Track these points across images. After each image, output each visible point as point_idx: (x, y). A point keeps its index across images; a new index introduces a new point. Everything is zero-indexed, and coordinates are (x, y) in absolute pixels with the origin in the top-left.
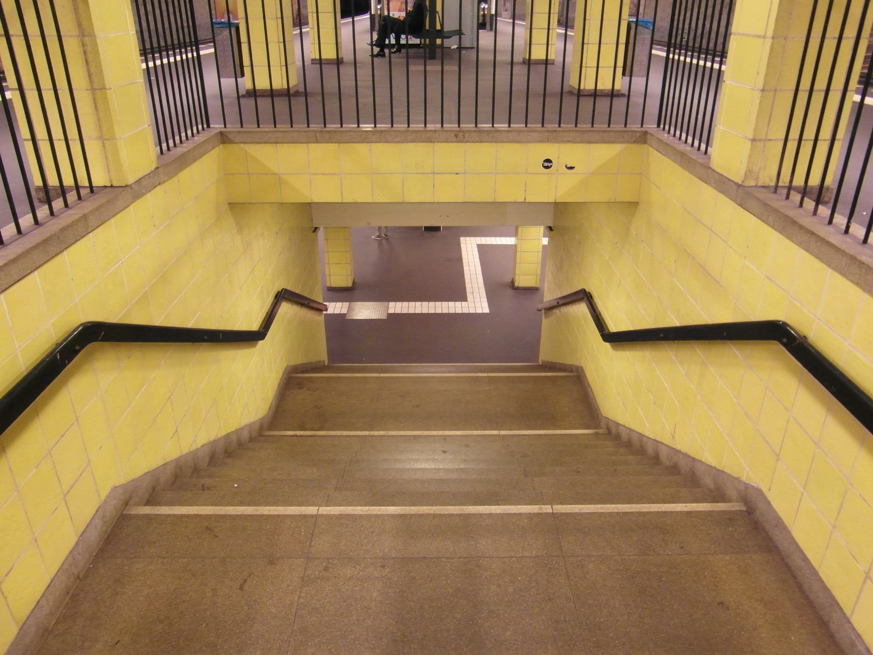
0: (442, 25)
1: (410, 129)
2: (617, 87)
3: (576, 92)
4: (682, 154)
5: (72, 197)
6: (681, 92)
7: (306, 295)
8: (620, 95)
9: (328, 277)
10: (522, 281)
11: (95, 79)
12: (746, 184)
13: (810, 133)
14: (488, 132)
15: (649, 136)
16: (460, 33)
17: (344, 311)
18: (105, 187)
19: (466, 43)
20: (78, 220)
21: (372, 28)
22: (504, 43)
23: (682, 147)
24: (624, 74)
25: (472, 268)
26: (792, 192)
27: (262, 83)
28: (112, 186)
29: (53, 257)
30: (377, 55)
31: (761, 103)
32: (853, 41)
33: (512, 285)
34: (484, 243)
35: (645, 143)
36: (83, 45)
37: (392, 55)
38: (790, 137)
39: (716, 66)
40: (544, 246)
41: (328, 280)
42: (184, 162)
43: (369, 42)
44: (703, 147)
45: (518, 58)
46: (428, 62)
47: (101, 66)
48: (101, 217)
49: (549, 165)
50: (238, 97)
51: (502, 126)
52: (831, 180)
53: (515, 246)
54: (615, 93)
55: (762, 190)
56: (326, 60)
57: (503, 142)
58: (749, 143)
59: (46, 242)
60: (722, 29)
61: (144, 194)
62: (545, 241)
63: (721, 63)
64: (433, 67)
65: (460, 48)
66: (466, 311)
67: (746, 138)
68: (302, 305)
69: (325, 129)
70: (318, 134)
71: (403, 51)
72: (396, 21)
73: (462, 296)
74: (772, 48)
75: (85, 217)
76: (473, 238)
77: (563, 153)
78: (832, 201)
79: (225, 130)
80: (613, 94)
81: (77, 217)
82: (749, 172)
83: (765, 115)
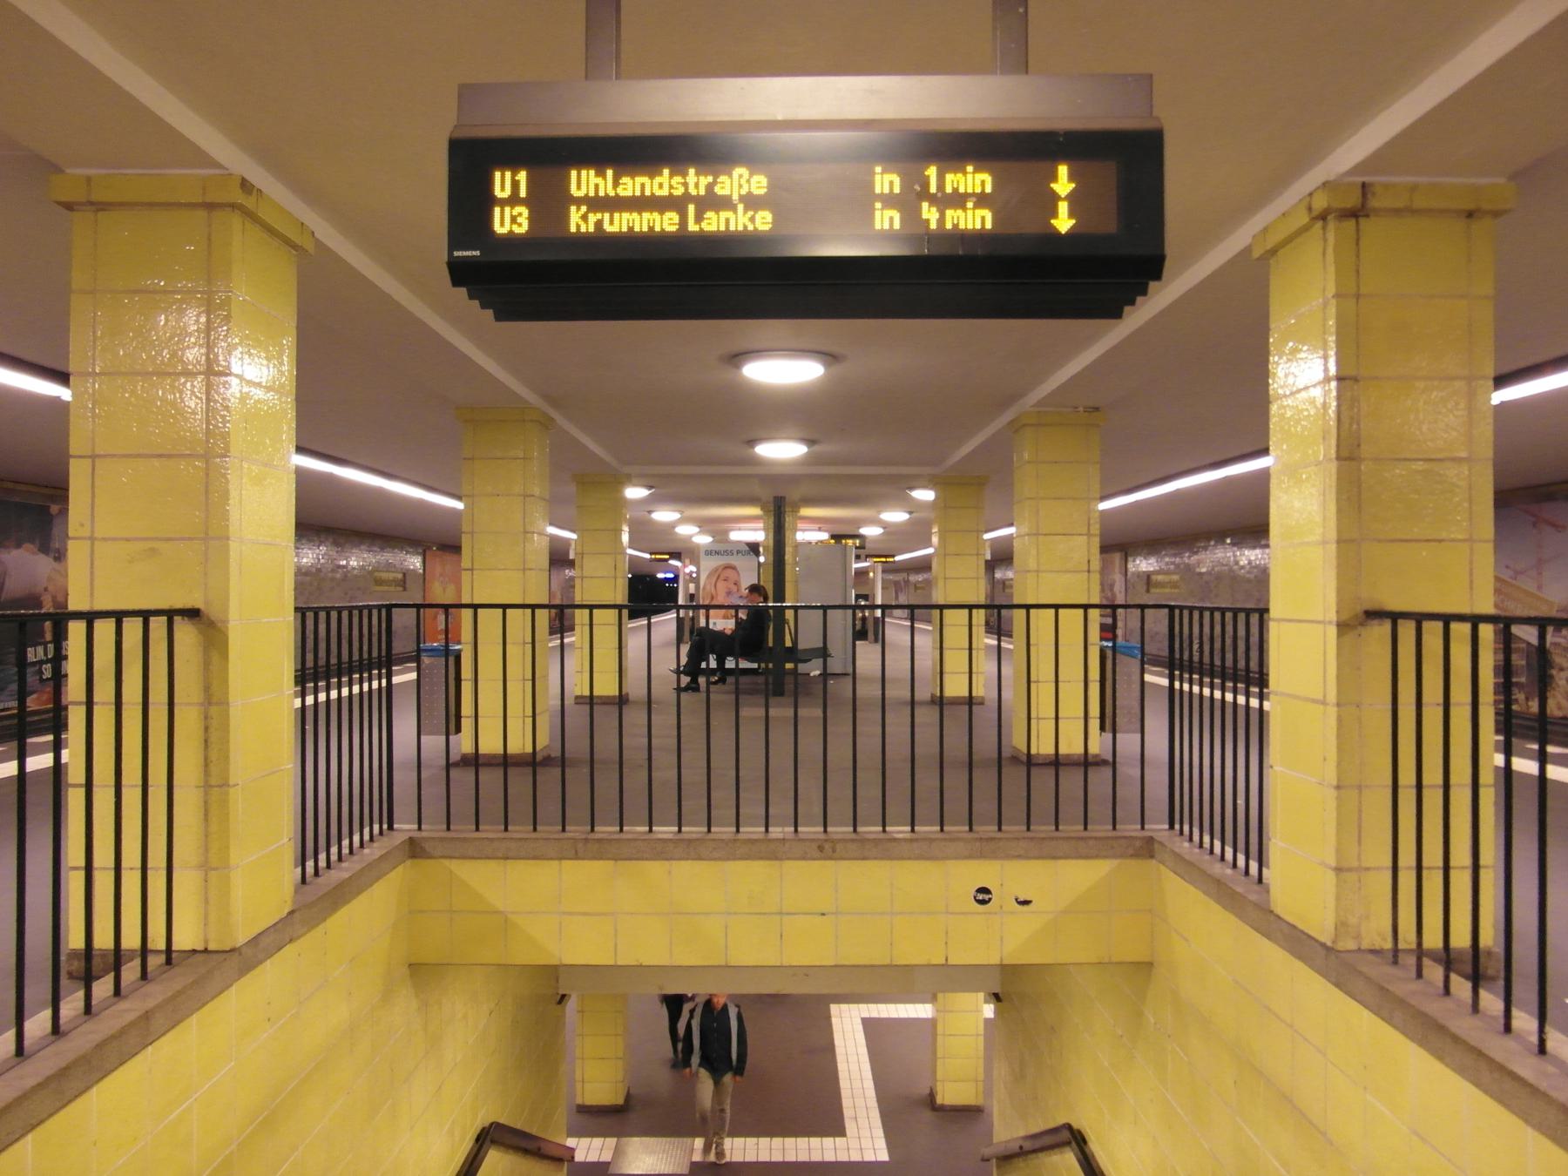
0: (795, 642)
1: (740, 836)
2: (1094, 748)
3: (1024, 758)
4: (1218, 882)
5: (130, 972)
6: (1202, 753)
7: (534, 1131)
8: (1100, 762)
9: (579, 1086)
10: (950, 1094)
11: (213, 769)
12: (1341, 946)
13: (1433, 856)
14: (876, 842)
15: (1156, 846)
16: (823, 653)
17: (606, 1157)
18: (194, 951)
19: (835, 665)
20: (132, 1024)
21: (679, 640)
22: (898, 665)
23: (1217, 869)
24: (1102, 728)
25: (854, 1067)
26: (1426, 962)
27: (491, 744)
28: (206, 951)
29: (70, 1102)
30: (687, 689)
31: (1339, 807)
32: (1468, 710)
33: (930, 1101)
34: (875, 1015)
35: (1152, 857)
36: (206, 718)
37: (712, 688)
38: (1401, 863)
39: (1254, 703)
40: (987, 1021)
41: (579, 1093)
42: (340, 896)
43: (674, 666)
44: (1254, 866)
45: (923, 694)
46: (772, 700)
47: (228, 751)
48: (175, 1012)
49: (986, 897)
50: (448, 766)
51: (900, 830)
52: (1490, 937)
53: (932, 1023)
54: (1090, 759)
55: (1370, 957)
56: (600, 697)
57: (903, 858)
58: (1331, 875)
59: (63, 1073)
60: (1254, 639)
61: (261, 962)
62: (989, 1010)
63: (1261, 697)
64: (781, 711)
65: (825, 675)
66: (843, 1157)
67: (1323, 864)
68: (526, 1152)
69: (592, 836)
70: (580, 845)
71: (730, 679)
72: (720, 635)
73: (833, 1125)
74: (1340, 720)
75: (147, 1016)
76: (853, 1006)
77: (1011, 876)
78: (1502, 974)
79: (417, 834)
80: (1086, 762)
81: (131, 1017)
82: (1341, 926)
83: (1350, 825)
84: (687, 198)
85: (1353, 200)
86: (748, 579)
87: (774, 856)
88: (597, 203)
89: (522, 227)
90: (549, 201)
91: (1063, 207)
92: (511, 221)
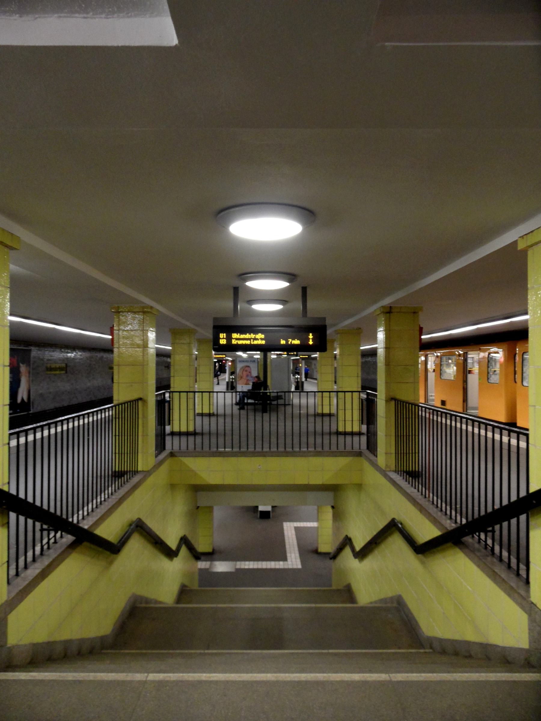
8: (333, 415)
33: (316, 552)
53: (317, 528)
64: (266, 416)
66: (286, 567)
74: (386, 422)
84: (251, 338)
85: (388, 310)
86: (255, 373)
87: (265, 456)
88: (237, 339)
89: (225, 343)
90: (229, 339)
91: (311, 340)
92: (223, 342)
